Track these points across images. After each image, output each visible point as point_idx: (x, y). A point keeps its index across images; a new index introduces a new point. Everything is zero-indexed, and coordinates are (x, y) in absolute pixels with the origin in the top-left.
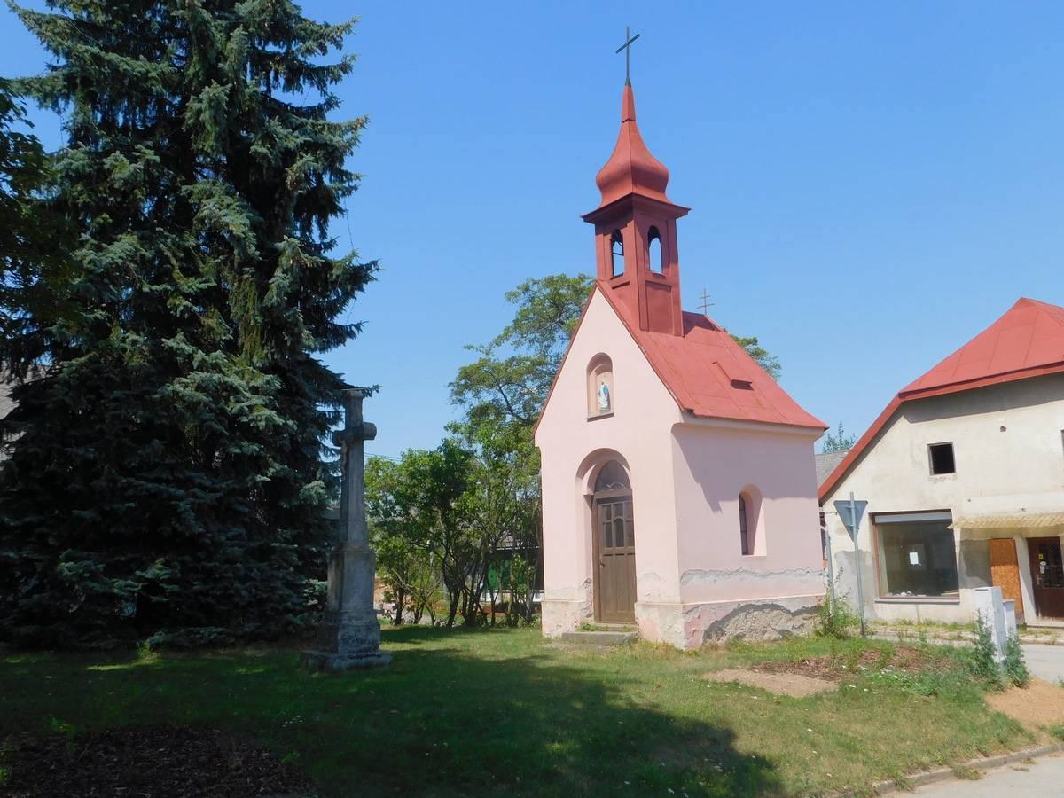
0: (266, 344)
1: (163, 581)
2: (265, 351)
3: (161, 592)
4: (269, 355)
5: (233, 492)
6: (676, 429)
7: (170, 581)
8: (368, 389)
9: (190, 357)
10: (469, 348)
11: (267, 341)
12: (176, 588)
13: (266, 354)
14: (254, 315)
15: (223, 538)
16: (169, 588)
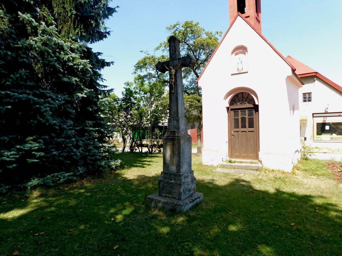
0: (77, 27)
1: (35, 151)
2: (77, 31)
3: (34, 157)
4: (80, 33)
5: (67, 102)
6: (289, 78)
7: (39, 150)
8: (109, 63)
9: (35, 29)
10: (141, 52)
11: (78, 26)
12: (42, 154)
13: (78, 33)
14: (71, 10)
15: (65, 126)
16: (38, 154)
